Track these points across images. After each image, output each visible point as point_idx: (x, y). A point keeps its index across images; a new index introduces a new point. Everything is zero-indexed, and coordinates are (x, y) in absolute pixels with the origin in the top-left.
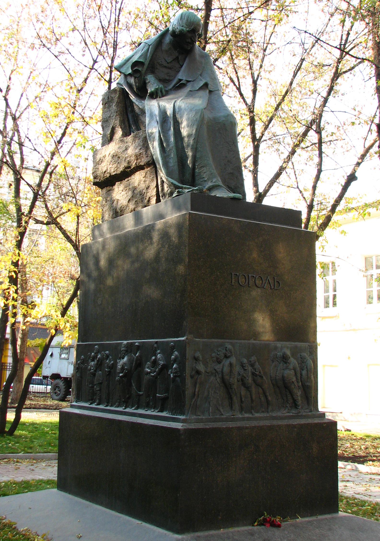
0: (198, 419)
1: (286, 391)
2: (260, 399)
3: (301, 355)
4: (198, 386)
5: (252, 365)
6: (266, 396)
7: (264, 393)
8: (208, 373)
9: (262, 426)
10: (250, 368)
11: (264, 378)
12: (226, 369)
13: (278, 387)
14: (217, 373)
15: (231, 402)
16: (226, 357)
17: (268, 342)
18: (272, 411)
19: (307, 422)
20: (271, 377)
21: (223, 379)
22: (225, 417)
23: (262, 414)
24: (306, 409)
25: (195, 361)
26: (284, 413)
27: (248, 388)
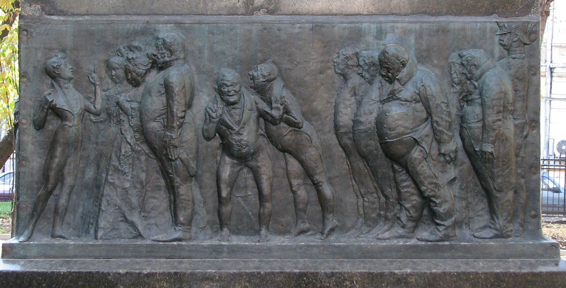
0: (52, 246)
1: (394, 171)
2: (294, 192)
3: (461, 56)
4: (59, 149)
5: (262, 90)
6: (316, 185)
7: (308, 173)
8: (97, 114)
9: (266, 274)
10: (250, 99)
11: (306, 127)
12: (156, 103)
13: (364, 157)
14: (126, 113)
15: (175, 201)
16: (158, 65)
17: (321, 19)
18: (342, 229)
19: (463, 268)
20: (336, 127)
21: (143, 133)
22: (149, 242)
23: (302, 237)
24: (484, 227)
25: (49, 81)
26: (386, 236)
27: (243, 159)
